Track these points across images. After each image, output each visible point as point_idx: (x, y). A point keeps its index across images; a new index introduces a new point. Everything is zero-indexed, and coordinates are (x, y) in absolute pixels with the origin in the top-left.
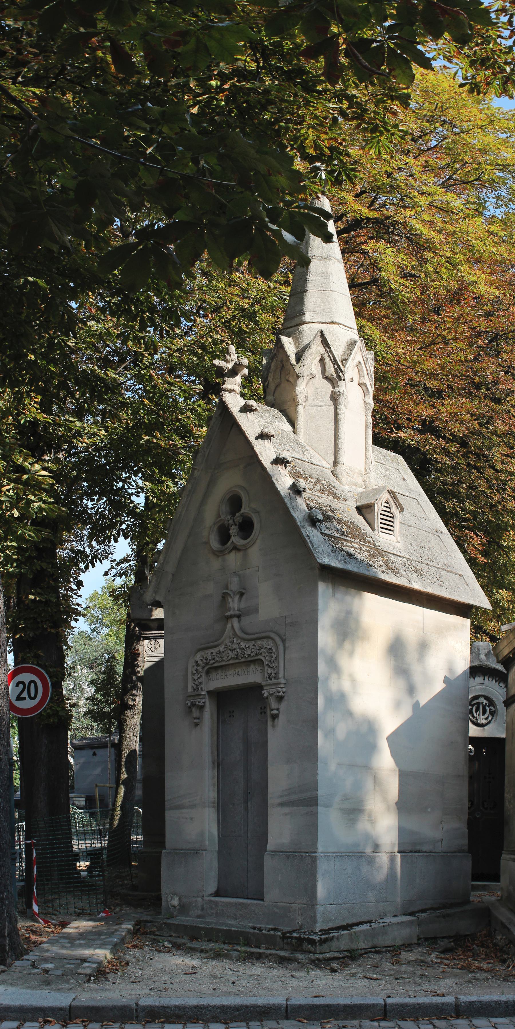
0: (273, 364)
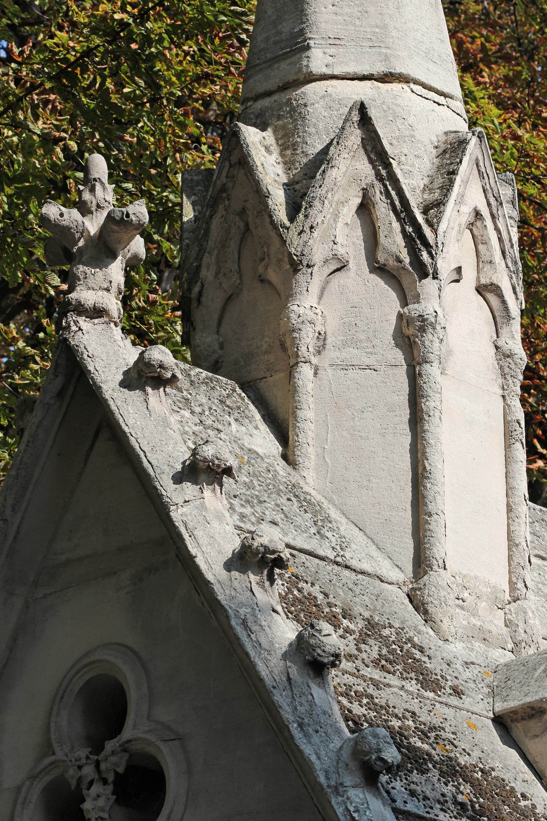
0: (215, 222)
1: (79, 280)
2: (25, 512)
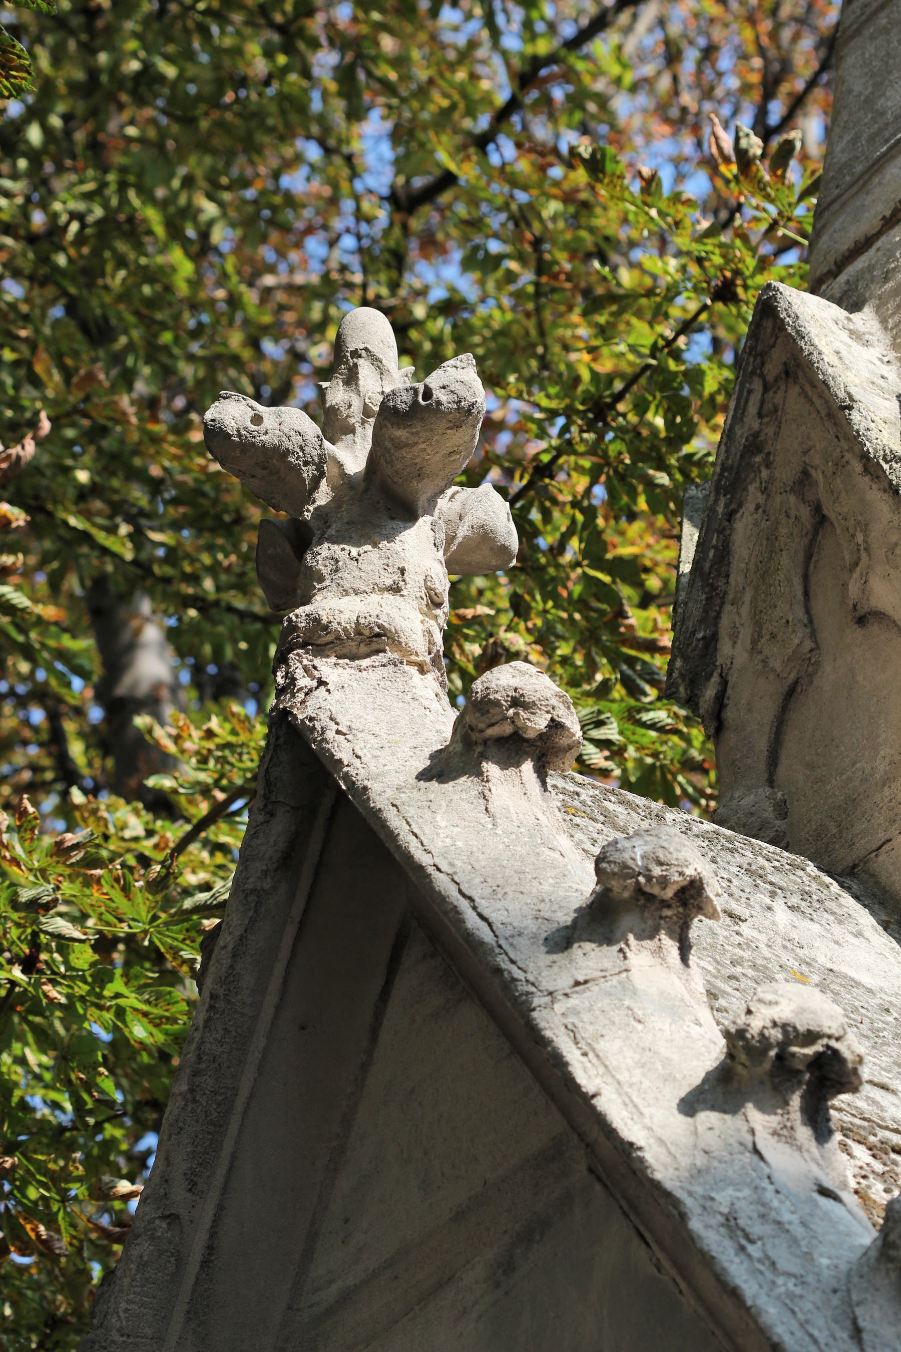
1: (321, 579)
2: (225, 1189)
